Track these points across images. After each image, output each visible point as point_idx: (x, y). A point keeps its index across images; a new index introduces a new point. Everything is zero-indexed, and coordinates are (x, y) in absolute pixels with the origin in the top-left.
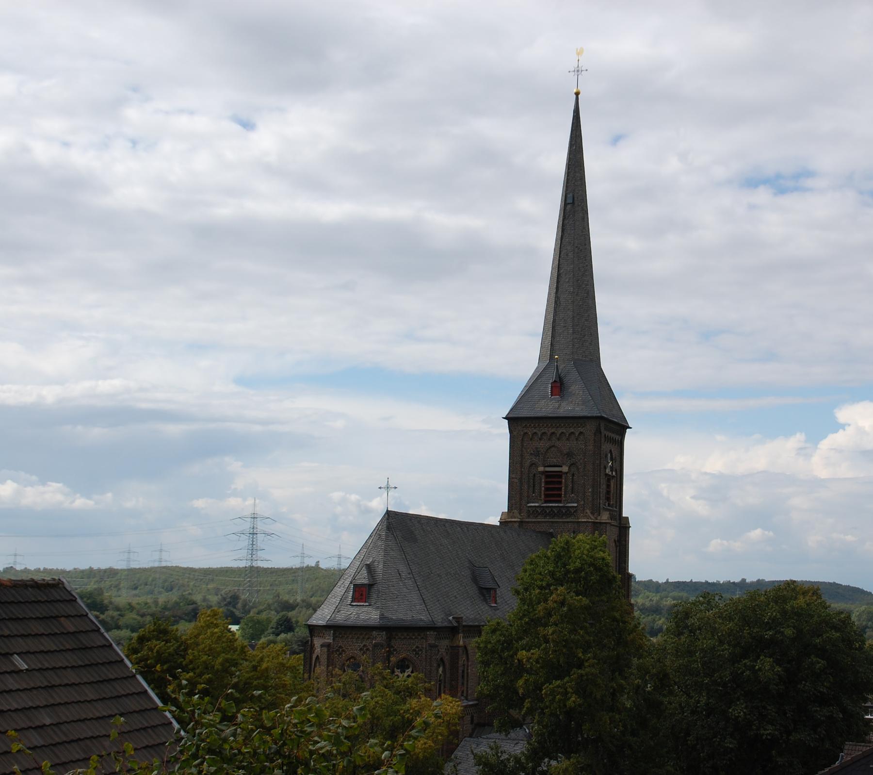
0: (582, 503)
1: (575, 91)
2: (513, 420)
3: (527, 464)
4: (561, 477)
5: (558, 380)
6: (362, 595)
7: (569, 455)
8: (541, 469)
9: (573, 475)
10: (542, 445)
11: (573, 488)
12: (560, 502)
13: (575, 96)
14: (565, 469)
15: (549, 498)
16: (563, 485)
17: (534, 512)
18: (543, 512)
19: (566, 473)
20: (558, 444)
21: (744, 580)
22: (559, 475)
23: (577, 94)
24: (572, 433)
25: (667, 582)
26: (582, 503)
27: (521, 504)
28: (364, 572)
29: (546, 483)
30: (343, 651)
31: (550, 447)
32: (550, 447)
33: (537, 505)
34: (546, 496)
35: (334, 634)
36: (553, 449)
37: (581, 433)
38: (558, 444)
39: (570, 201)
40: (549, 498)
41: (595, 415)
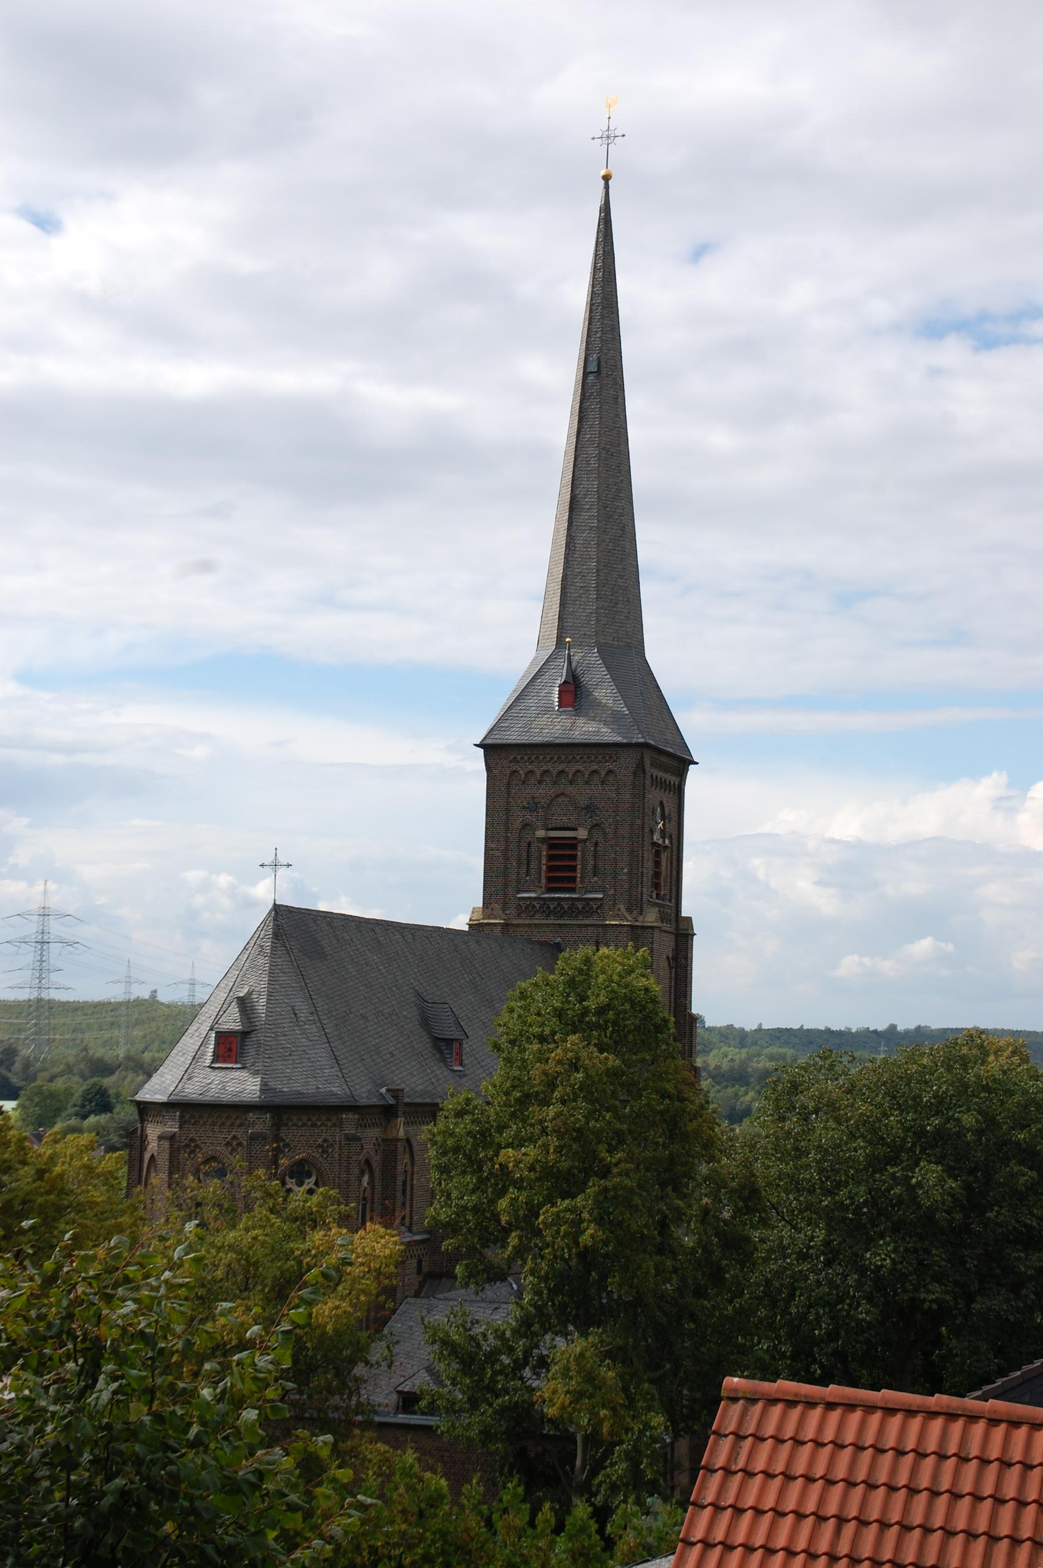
0: (612, 892)
1: (603, 172)
2: (493, 750)
3: (517, 824)
4: (574, 847)
5: (571, 680)
6: (230, 1050)
7: (590, 809)
8: (541, 833)
9: (596, 844)
10: (543, 792)
11: (595, 866)
12: (573, 890)
13: (603, 182)
14: (582, 834)
16: (579, 861)
17: (528, 908)
18: (544, 907)
19: (585, 841)
20: (569, 790)
21: (893, 1027)
22: (572, 844)
23: (607, 178)
24: (595, 772)
25: (759, 1030)
26: (612, 892)
27: (505, 894)
29: (550, 858)
30: (197, 1146)
31: (558, 796)
32: (558, 796)
33: (533, 895)
34: (550, 879)
35: (181, 1117)
36: (560, 799)
37: (610, 771)
38: (569, 790)
39: (593, 367)
41: (634, 741)
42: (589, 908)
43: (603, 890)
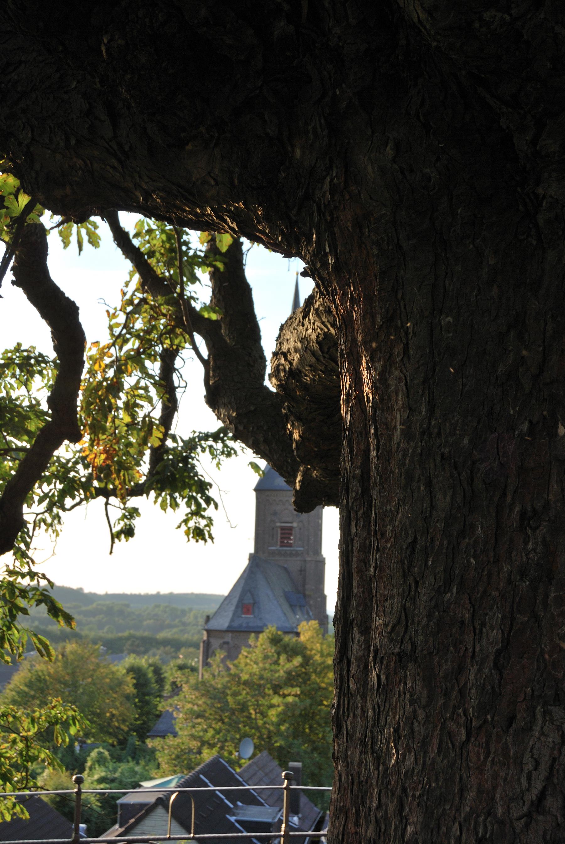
8: (278, 524)
14: (295, 525)
15: (283, 545)
21: (158, 593)
22: (291, 529)
28: (249, 595)
40: (283, 545)
42: (297, 554)
43: (303, 547)
